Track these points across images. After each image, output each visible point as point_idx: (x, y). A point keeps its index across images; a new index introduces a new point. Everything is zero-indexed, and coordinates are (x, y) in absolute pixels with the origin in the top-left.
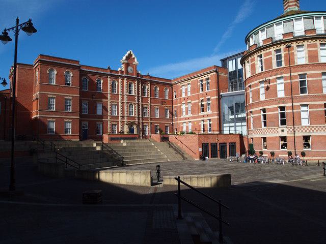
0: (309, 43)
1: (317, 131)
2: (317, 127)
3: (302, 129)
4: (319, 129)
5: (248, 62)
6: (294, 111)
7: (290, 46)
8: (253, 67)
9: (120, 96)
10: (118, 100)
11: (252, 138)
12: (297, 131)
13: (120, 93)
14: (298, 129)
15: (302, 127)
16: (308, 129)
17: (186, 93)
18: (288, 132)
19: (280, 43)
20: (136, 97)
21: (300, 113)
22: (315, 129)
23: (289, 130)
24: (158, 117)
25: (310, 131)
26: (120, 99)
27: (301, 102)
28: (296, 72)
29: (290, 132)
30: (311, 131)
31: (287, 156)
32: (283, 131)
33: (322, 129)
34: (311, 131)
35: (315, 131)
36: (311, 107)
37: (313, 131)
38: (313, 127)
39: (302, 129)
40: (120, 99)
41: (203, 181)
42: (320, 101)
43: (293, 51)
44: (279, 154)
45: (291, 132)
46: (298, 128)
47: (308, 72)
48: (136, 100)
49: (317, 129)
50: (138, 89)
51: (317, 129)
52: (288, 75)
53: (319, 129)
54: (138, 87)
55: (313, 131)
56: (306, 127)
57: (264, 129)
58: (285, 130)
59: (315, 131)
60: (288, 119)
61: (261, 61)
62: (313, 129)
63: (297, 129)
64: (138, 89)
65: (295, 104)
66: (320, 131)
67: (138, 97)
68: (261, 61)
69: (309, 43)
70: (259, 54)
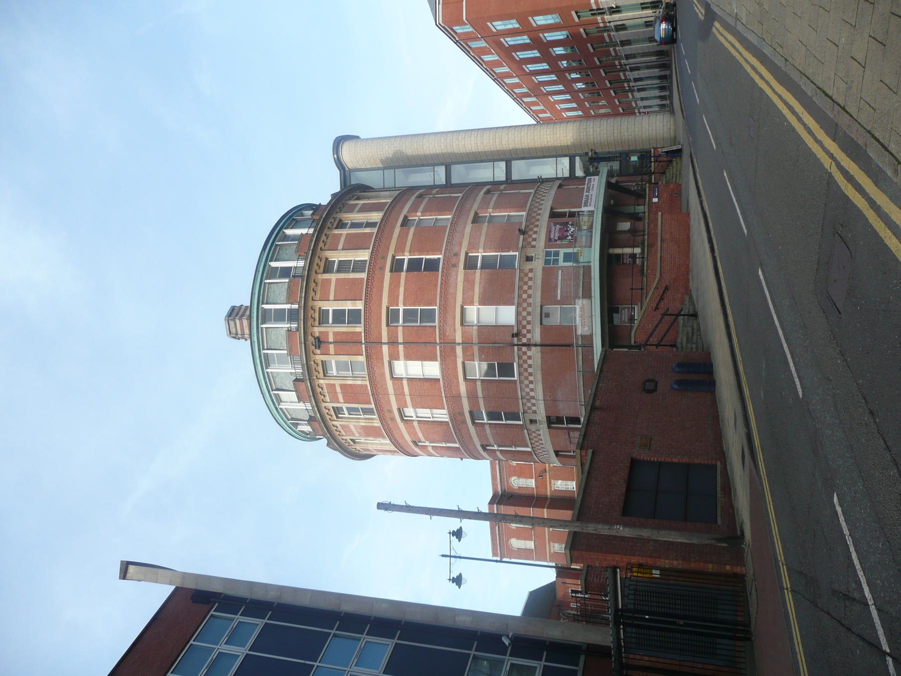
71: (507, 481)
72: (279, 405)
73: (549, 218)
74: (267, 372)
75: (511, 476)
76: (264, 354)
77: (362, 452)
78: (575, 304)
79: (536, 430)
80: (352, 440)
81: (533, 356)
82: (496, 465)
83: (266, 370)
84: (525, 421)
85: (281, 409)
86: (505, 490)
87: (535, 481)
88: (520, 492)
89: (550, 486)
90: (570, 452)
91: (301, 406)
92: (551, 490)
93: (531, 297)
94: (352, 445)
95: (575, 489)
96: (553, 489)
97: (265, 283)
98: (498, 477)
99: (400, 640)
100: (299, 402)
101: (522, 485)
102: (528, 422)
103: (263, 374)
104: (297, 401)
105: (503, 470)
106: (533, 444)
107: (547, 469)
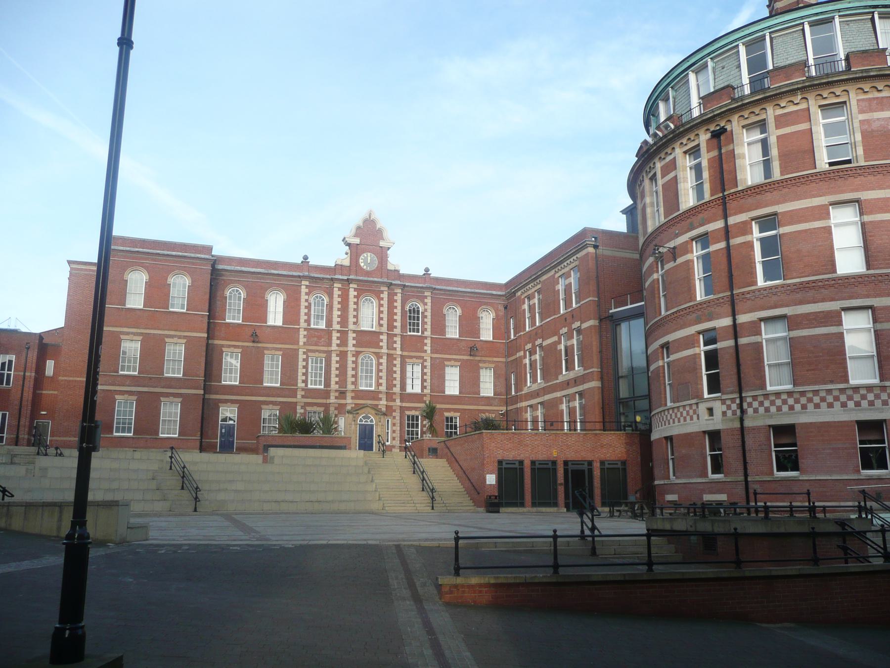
0: (780, 112)
1: (817, 406)
2: (816, 392)
3: (767, 404)
4: (823, 399)
5: (653, 178)
6: (742, 341)
7: (723, 130)
8: (672, 192)
9: (335, 335)
10: (330, 344)
11: (669, 439)
12: (750, 411)
13: (336, 327)
14: (755, 404)
15: (766, 396)
16: (785, 402)
17: (568, 303)
18: (724, 413)
19: (704, 122)
20: (384, 337)
21: (758, 347)
22: (810, 400)
23: (729, 407)
24: (456, 392)
25: (791, 408)
26: (335, 341)
27: (763, 308)
28: (741, 212)
29: (729, 413)
30: (798, 407)
31: (807, 515)
32: (710, 411)
33: (836, 399)
34: (798, 407)
35: (810, 406)
36: (793, 322)
37: (804, 407)
38: (803, 394)
39: (767, 404)
40: (335, 341)
41: (426, 501)
42: (823, 300)
43: (731, 147)
44: (703, 491)
45: (734, 413)
46: (755, 398)
47: (780, 208)
48: (384, 344)
49: (816, 400)
50: (391, 314)
51: (816, 400)
52: (720, 224)
53: (823, 399)
54: (391, 307)
55: (804, 407)
56: (778, 394)
57: (673, 408)
58: (718, 407)
59: (810, 406)
60: (726, 370)
61: (764, 143)
62: (803, 400)
63: (750, 405)
64: (391, 314)
65: (742, 319)
66: (817, 406)
67: (390, 337)
68: (764, 143)
69: (780, 112)
70: (754, 119)
71: (239, 282)
72: (693, 71)
73: (856, 421)
74: (738, 45)
75: (247, 287)
76: (764, 36)
77: (639, 188)
78: (126, 347)
79: (698, 415)
80: (655, 174)
81: (781, 414)
82: (264, 268)
83: (740, 43)
84: (708, 400)
85: (688, 74)
86: (221, 275)
87: (239, 324)
88: (218, 298)
89: (229, 346)
90: (673, 454)
91: (695, 101)
92: (223, 346)
93: (829, 407)
94: (647, 175)
95: (223, 383)
96: (224, 349)
97: (873, 13)
98: (244, 269)
99: (761, 333)
100: (700, 98)
101: (230, 303)
102: (709, 405)
103: (736, 40)
104: (701, 96)
105: (258, 279)
106: (684, 409)
107: (260, 345)
